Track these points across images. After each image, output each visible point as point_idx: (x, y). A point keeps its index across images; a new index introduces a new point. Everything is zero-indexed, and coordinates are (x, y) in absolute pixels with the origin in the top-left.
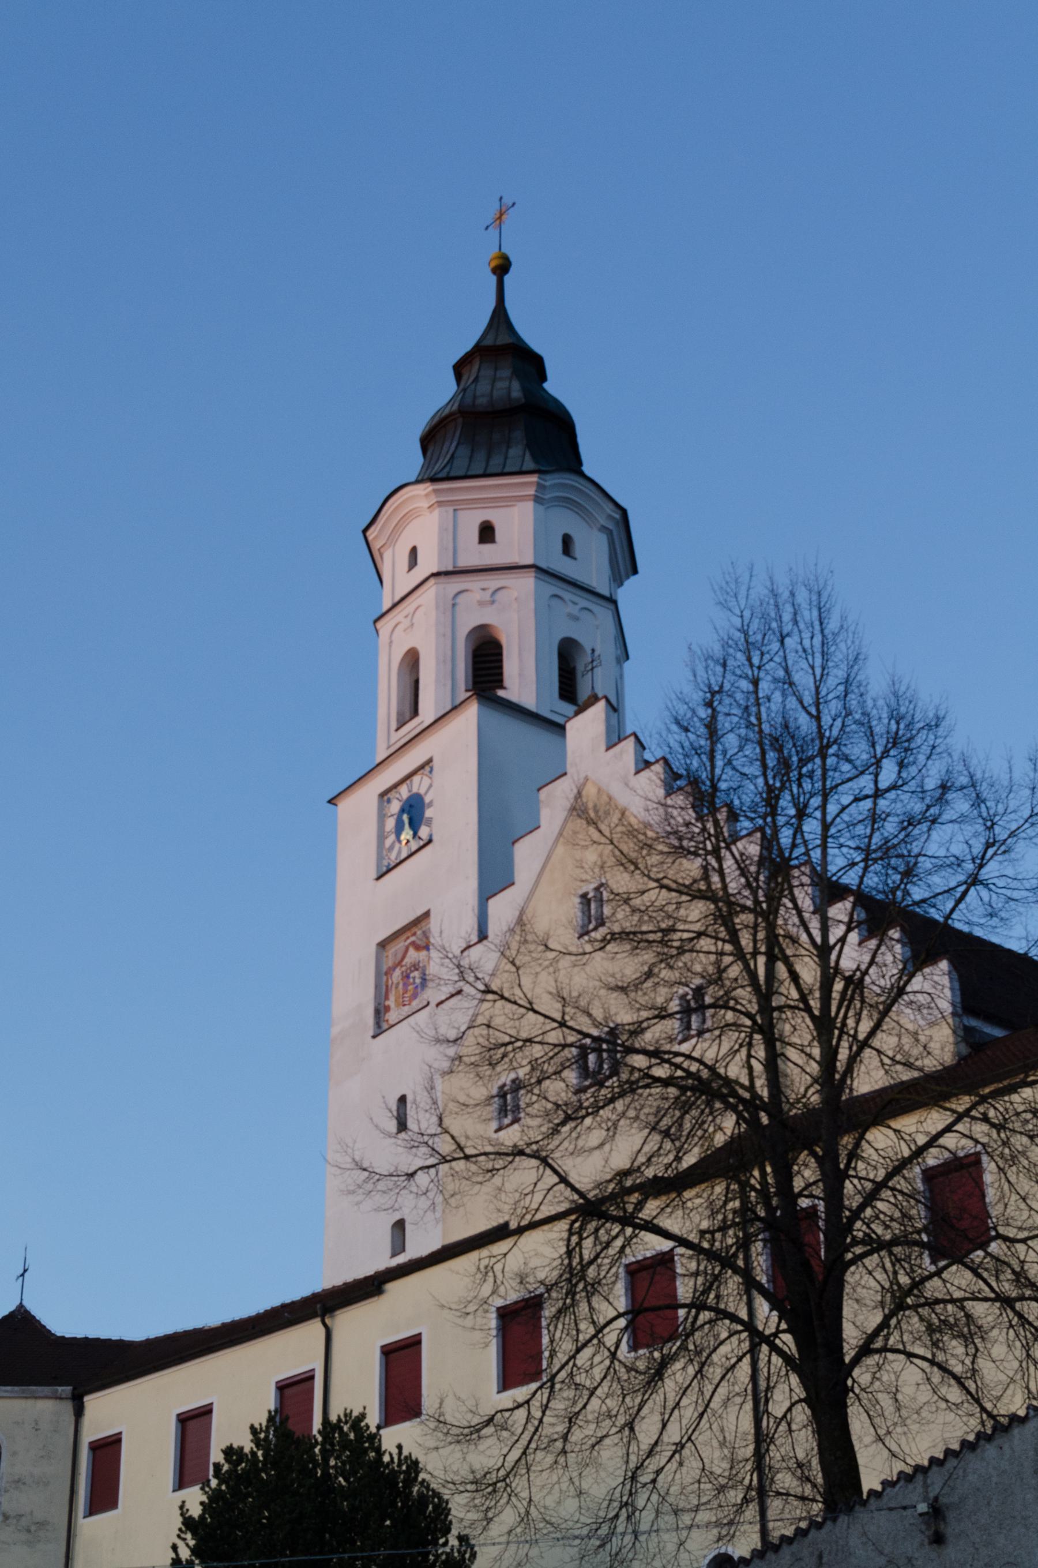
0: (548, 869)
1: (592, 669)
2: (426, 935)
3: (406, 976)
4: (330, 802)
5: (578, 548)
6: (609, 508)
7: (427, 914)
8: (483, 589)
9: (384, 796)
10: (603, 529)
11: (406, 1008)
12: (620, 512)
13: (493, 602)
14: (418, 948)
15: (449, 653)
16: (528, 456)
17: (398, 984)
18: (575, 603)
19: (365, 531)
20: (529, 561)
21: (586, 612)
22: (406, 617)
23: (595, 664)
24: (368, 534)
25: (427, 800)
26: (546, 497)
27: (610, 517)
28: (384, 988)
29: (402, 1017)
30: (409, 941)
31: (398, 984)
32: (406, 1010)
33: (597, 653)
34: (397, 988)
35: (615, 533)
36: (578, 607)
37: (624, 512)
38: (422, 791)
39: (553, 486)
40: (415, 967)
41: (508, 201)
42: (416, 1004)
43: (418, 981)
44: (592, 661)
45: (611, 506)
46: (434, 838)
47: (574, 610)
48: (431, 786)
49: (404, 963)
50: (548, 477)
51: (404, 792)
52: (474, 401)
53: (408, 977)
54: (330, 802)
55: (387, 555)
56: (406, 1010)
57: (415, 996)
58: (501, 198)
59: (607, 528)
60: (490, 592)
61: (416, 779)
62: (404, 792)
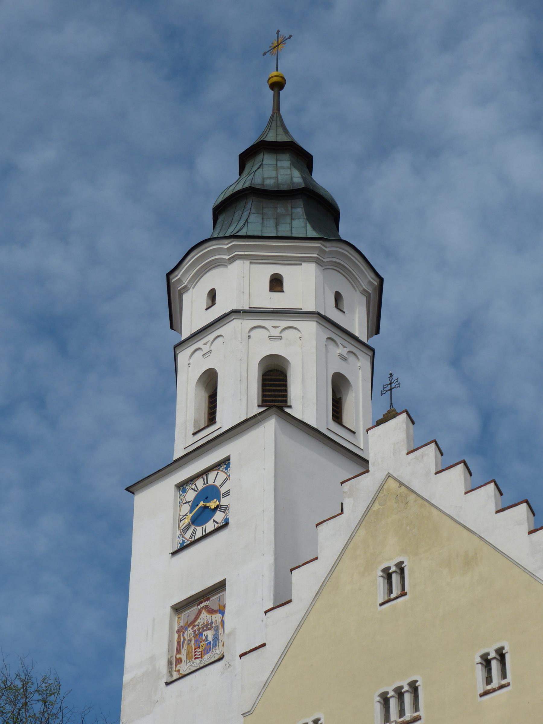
0: (351, 546)
1: (391, 390)
2: (221, 600)
3: (198, 635)
4: (127, 489)
5: (346, 304)
6: (370, 276)
7: (221, 586)
8: (274, 327)
9: (182, 486)
10: (364, 292)
11: (198, 661)
12: (378, 280)
13: (281, 338)
14: (211, 611)
15: (245, 374)
16: (309, 227)
17: (190, 640)
18: (345, 347)
19: (169, 275)
20: (311, 308)
21: (353, 355)
22: (205, 344)
23: (393, 385)
24: (171, 277)
25: (223, 490)
26: (325, 260)
27: (370, 282)
28: (176, 643)
29: (193, 669)
30: (202, 605)
31: (190, 640)
32: (198, 663)
33: (394, 378)
34: (189, 644)
35: (372, 296)
36: (347, 350)
37: (381, 280)
38: (218, 483)
39: (330, 252)
40: (208, 626)
41: (284, 33)
42: (208, 658)
43: (210, 638)
44: (391, 384)
45: (372, 275)
46: (231, 521)
47: (344, 352)
48: (226, 480)
49: (196, 623)
50: (327, 244)
51: (200, 484)
52: (263, 182)
53: (201, 634)
54: (127, 489)
55: (186, 297)
56: (198, 663)
57: (207, 650)
58: (278, 32)
59: (368, 292)
60: (279, 329)
61: (212, 476)
62: (200, 484)
